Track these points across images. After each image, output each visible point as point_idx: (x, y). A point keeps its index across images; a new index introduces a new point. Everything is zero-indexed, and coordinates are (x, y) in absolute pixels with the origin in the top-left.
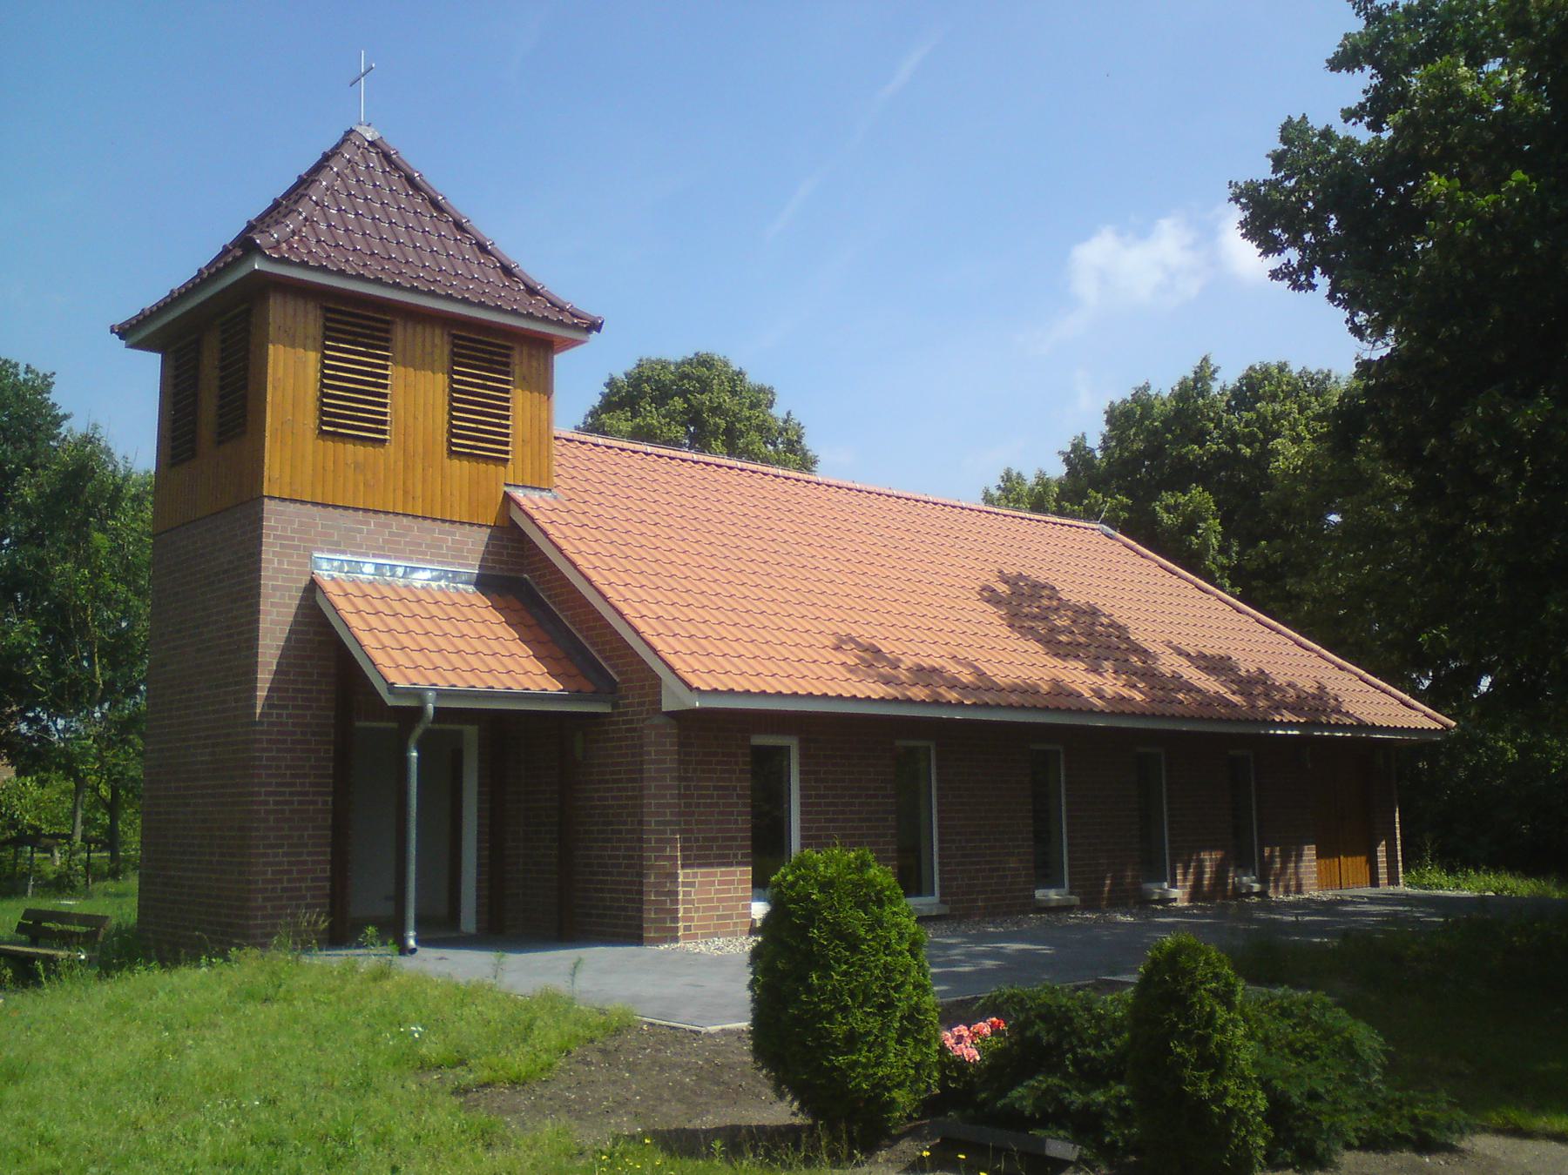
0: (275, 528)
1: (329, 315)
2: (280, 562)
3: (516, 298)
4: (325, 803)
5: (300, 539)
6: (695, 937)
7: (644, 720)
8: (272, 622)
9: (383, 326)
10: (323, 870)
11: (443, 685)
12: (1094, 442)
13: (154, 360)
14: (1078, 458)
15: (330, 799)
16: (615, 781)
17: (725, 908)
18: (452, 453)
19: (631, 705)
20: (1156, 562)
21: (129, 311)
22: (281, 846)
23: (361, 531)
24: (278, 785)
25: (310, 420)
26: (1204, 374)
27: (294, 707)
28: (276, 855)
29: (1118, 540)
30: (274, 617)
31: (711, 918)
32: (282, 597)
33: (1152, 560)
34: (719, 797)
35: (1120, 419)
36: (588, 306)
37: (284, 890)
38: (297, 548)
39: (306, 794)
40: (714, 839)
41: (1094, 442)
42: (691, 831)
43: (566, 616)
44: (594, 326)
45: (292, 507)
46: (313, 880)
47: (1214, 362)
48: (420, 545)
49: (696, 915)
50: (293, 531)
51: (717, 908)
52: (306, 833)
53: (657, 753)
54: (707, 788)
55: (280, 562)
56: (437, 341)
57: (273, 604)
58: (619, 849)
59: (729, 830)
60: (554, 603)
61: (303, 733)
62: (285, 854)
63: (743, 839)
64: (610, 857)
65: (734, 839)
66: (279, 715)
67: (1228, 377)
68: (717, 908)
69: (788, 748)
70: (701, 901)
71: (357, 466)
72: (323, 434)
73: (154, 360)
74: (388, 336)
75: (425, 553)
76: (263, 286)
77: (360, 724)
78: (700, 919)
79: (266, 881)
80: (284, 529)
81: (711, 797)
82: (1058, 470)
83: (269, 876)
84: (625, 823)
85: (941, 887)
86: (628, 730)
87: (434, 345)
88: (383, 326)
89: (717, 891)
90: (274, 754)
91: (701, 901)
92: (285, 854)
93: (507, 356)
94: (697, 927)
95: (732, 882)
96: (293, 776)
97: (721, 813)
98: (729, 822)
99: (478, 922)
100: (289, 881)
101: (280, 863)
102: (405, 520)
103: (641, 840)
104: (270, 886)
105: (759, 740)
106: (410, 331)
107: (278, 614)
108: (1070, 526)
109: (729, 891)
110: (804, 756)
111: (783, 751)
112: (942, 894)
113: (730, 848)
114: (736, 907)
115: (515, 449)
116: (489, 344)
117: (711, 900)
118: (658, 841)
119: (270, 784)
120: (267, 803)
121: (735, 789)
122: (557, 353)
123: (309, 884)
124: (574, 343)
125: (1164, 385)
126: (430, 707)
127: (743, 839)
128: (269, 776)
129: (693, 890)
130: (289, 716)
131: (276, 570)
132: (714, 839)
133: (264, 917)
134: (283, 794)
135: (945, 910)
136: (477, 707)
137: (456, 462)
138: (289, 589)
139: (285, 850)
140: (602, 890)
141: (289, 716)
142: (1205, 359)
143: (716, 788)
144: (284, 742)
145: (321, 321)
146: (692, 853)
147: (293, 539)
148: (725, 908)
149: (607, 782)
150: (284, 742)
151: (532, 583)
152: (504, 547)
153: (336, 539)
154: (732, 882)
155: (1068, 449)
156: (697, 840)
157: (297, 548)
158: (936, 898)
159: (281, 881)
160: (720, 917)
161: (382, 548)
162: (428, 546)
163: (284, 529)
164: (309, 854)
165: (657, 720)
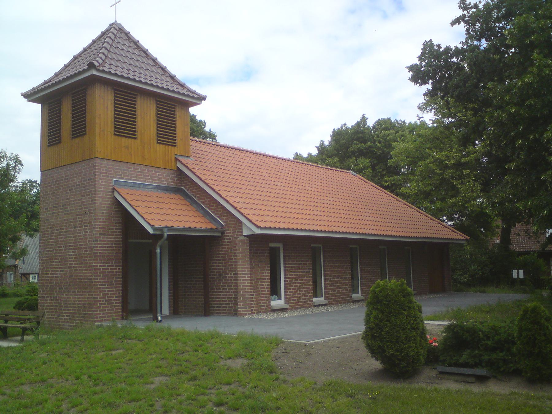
0: (100, 169)
1: (116, 92)
2: (102, 182)
3: (175, 88)
4: (119, 269)
5: (109, 174)
6: (254, 313)
7: (236, 238)
8: (101, 204)
9: (133, 96)
10: (119, 293)
11: (169, 226)
12: (326, 143)
13: (39, 106)
14: (322, 149)
15: (121, 268)
16: (223, 260)
17: (263, 303)
18: (158, 143)
19: (230, 233)
20: (371, 184)
21: (28, 87)
22: (105, 285)
23: (128, 171)
24: (104, 263)
25: (110, 128)
26: (364, 119)
27: (109, 235)
28: (103, 288)
29: (358, 177)
30: (101, 202)
31: (259, 307)
32: (103, 194)
33: (369, 183)
34: (261, 265)
35: (338, 135)
36: (200, 91)
37: (106, 301)
38: (108, 177)
39: (113, 266)
40: (259, 279)
41: (326, 143)
42: (252, 277)
43: (201, 202)
44: (204, 98)
45: (105, 162)
46: (116, 297)
47: (366, 116)
48: (148, 176)
49: (254, 306)
50: (106, 170)
51: (260, 303)
52: (113, 280)
53: (242, 249)
54: (256, 262)
55: (102, 182)
56: (152, 102)
57: (101, 197)
58: (226, 283)
59: (264, 276)
60: (193, 195)
61: (112, 244)
62: (106, 288)
63: (268, 279)
64: (222, 286)
65: (265, 279)
66: (103, 238)
67: (371, 123)
68: (260, 303)
69: (279, 248)
70: (256, 301)
71: (127, 147)
72: (115, 135)
73: (39, 106)
74: (135, 100)
75: (150, 179)
76: (94, 81)
77: (130, 241)
78: (256, 307)
79: (100, 298)
80: (103, 170)
81: (258, 265)
82: (315, 152)
83: (101, 296)
84: (228, 274)
85: (325, 294)
86: (228, 242)
87: (150, 104)
88: (133, 96)
89: (261, 297)
90: (102, 252)
91: (256, 301)
92: (106, 288)
93: (174, 108)
94: (255, 310)
95: (265, 294)
96: (108, 259)
97: (261, 270)
98: (263, 273)
99: (169, 310)
100: (108, 297)
101: (105, 291)
102: (143, 167)
103: (237, 280)
104: (102, 299)
105: (272, 245)
106: (142, 98)
107: (102, 201)
108: (343, 172)
109: (263, 297)
110: (284, 250)
111: (279, 248)
112: (325, 297)
113: (264, 282)
114: (266, 303)
115: (178, 141)
116: (169, 104)
117: (259, 300)
118: (243, 280)
119: (101, 263)
120: (100, 269)
121: (265, 262)
122: (190, 107)
123: (115, 298)
124: (196, 104)
125: (351, 123)
126: (165, 234)
127: (268, 279)
128: (100, 260)
129: (253, 297)
130: (107, 238)
131: (101, 185)
132: (259, 279)
133: (100, 311)
134: (105, 266)
135: (327, 302)
136: (175, 234)
137: (158, 145)
138: (105, 192)
139: (107, 286)
140: (219, 298)
141: (107, 238)
142: (364, 115)
143: (260, 261)
144: (105, 247)
145: (113, 94)
146: (227, 285)
147: (106, 173)
148: (263, 303)
149: (226, 259)
150: (105, 247)
151: (186, 190)
152: (176, 177)
153: (120, 173)
154: (265, 294)
155: (318, 145)
156: (254, 280)
157: (108, 177)
158: (323, 298)
159: (105, 298)
160: (262, 306)
161: (136, 177)
162: (151, 176)
163: (103, 170)
164: (115, 287)
165: (241, 238)
